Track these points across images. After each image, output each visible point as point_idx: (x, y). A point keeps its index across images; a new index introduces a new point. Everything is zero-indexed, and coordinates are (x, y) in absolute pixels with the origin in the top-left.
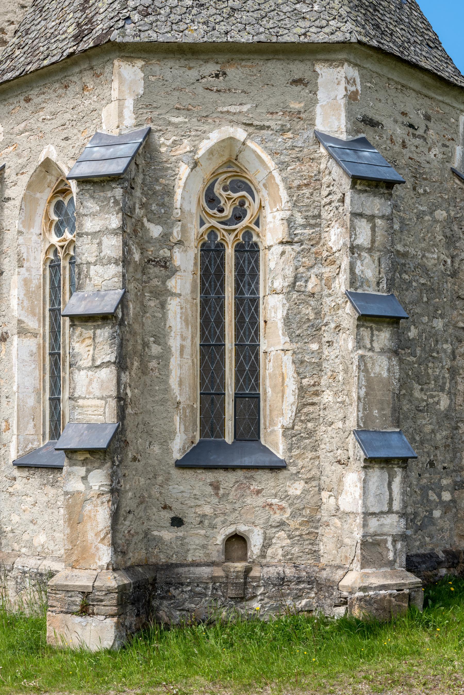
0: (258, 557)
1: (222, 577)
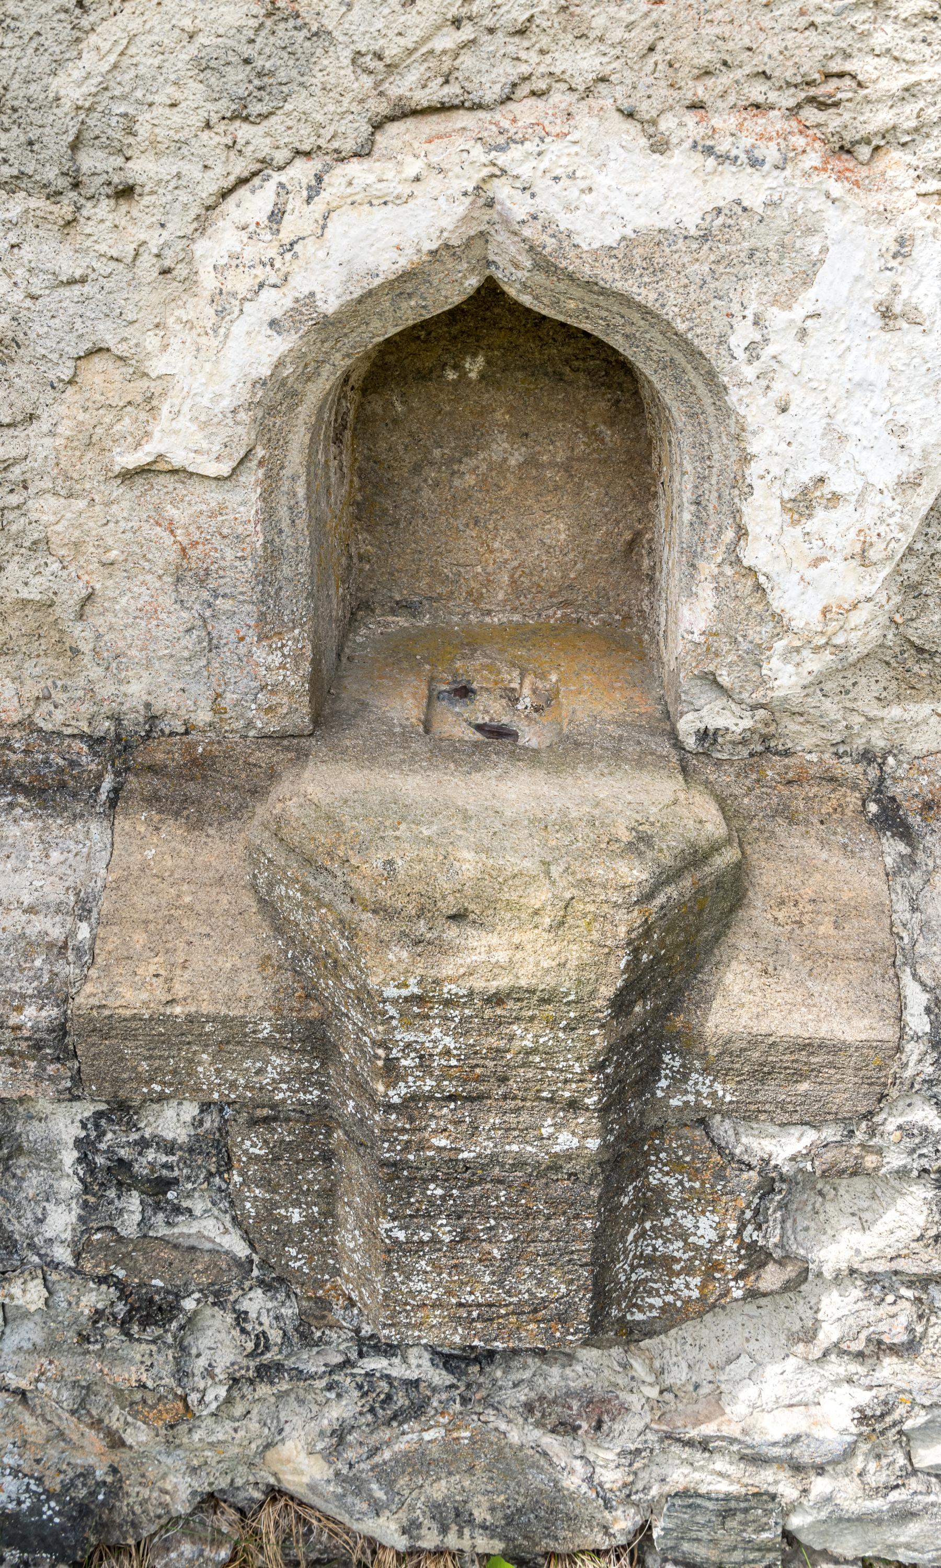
0: (848, 669)
1: (232, 1036)
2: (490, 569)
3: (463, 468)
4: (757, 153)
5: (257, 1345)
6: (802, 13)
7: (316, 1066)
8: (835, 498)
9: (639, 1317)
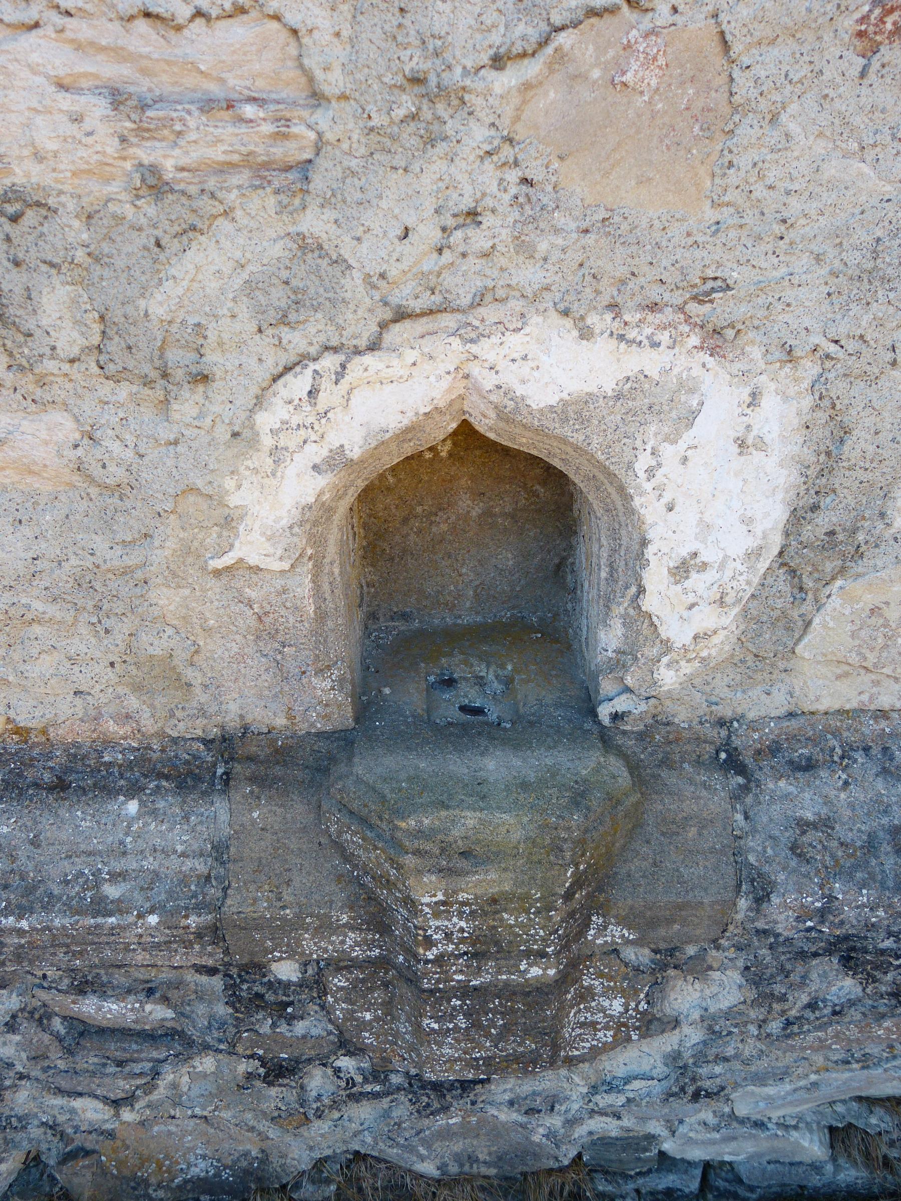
2: (460, 587)
3: (438, 519)
4: (656, 339)
5: (348, 1084)
6: (689, 234)
7: (378, 936)
8: (704, 566)
9: (576, 1053)
